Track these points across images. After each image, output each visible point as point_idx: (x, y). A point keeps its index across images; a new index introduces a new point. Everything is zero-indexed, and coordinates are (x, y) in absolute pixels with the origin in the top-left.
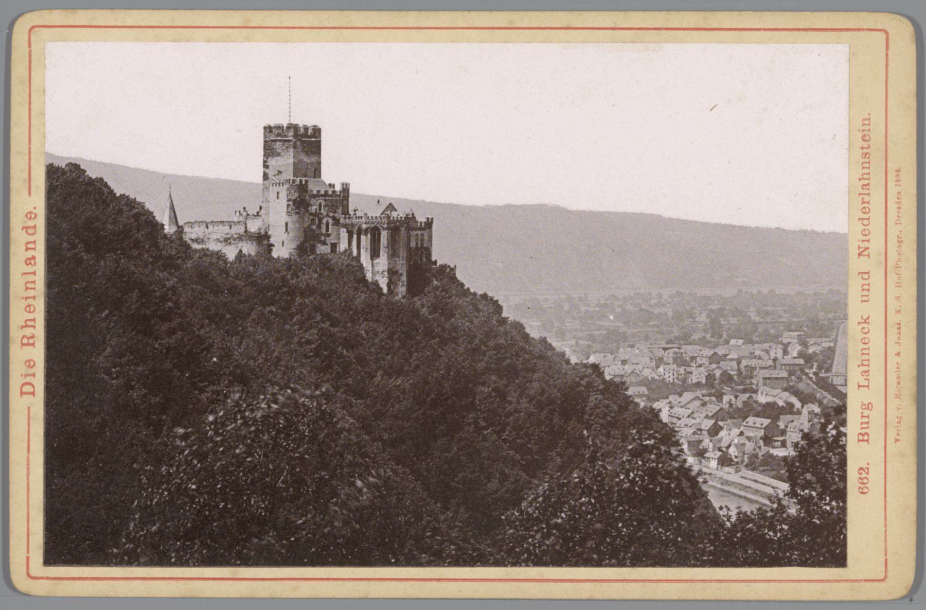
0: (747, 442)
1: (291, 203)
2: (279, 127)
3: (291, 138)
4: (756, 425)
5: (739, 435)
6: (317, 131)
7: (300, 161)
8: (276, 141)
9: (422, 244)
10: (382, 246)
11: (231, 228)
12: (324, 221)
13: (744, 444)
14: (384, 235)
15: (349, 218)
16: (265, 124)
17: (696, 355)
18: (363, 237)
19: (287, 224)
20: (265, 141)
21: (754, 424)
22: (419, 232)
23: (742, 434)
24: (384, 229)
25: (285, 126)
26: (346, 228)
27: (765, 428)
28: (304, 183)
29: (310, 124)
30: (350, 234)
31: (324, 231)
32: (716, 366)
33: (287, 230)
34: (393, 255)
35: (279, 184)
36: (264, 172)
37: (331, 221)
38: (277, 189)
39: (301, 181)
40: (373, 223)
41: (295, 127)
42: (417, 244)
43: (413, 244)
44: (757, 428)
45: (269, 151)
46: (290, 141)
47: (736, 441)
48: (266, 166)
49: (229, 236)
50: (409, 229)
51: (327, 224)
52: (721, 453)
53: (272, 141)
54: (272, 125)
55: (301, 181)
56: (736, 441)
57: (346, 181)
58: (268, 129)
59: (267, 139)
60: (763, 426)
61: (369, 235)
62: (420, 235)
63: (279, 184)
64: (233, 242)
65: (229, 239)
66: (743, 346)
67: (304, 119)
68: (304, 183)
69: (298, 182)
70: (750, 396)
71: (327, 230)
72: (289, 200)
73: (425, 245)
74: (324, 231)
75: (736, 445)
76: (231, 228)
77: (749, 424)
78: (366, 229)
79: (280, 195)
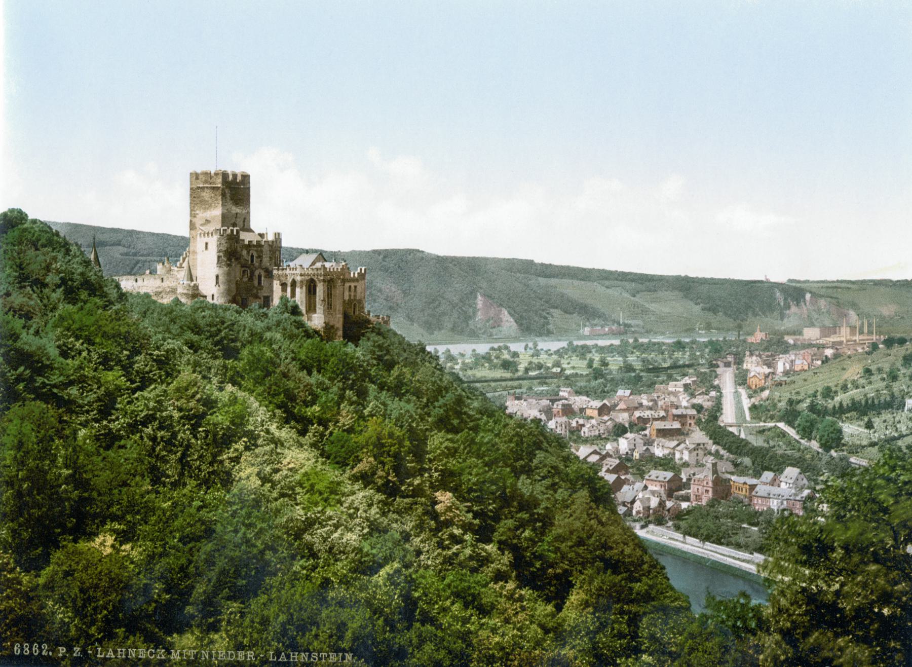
0: (652, 497)
1: (221, 254)
2: (206, 174)
3: (219, 185)
4: (659, 479)
5: (643, 490)
6: (246, 178)
7: (229, 211)
8: (203, 188)
9: (355, 296)
10: (317, 299)
11: (162, 281)
12: (257, 273)
13: (649, 499)
14: (320, 289)
15: (283, 269)
16: (192, 171)
17: (584, 407)
18: (298, 290)
19: (217, 277)
20: (191, 189)
21: (657, 477)
22: (353, 285)
23: (646, 487)
24: (320, 281)
25: (213, 173)
26: (280, 280)
27: (668, 482)
28: (235, 233)
29: (239, 170)
30: (284, 285)
31: (256, 282)
32: (608, 418)
33: (217, 283)
34: (329, 306)
35: (208, 233)
36: (191, 221)
37: (263, 273)
38: (206, 239)
39: (232, 231)
40: (308, 275)
41: (225, 175)
42: (350, 296)
43: (346, 298)
44: (652, 480)
45: (196, 196)
46: (218, 188)
47: (640, 495)
48: (193, 215)
49: (160, 290)
50: (344, 281)
51: (260, 277)
52: (626, 508)
53: (199, 188)
54: (199, 171)
55: (232, 231)
56: (640, 495)
57: (277, 231)
58: (195, 176)
59: (193, 186)
60: (667, 480)
61: (304, 288)
62: (353, 288)
63: (208, 233)
64: (164, 296)
65: (161, 293)
66: (631, 397)
67: (235, 166)
68: (235, 233)
69: (229, 231)
70: (647, 449)
71: (260, 283)
72: (219, 252)
73: (358, 298)
74: (256, 282)
75: (641, 501)
76: (162, 281)
77: (651, 478)
78: (301, 282)
79: (209, 246)
